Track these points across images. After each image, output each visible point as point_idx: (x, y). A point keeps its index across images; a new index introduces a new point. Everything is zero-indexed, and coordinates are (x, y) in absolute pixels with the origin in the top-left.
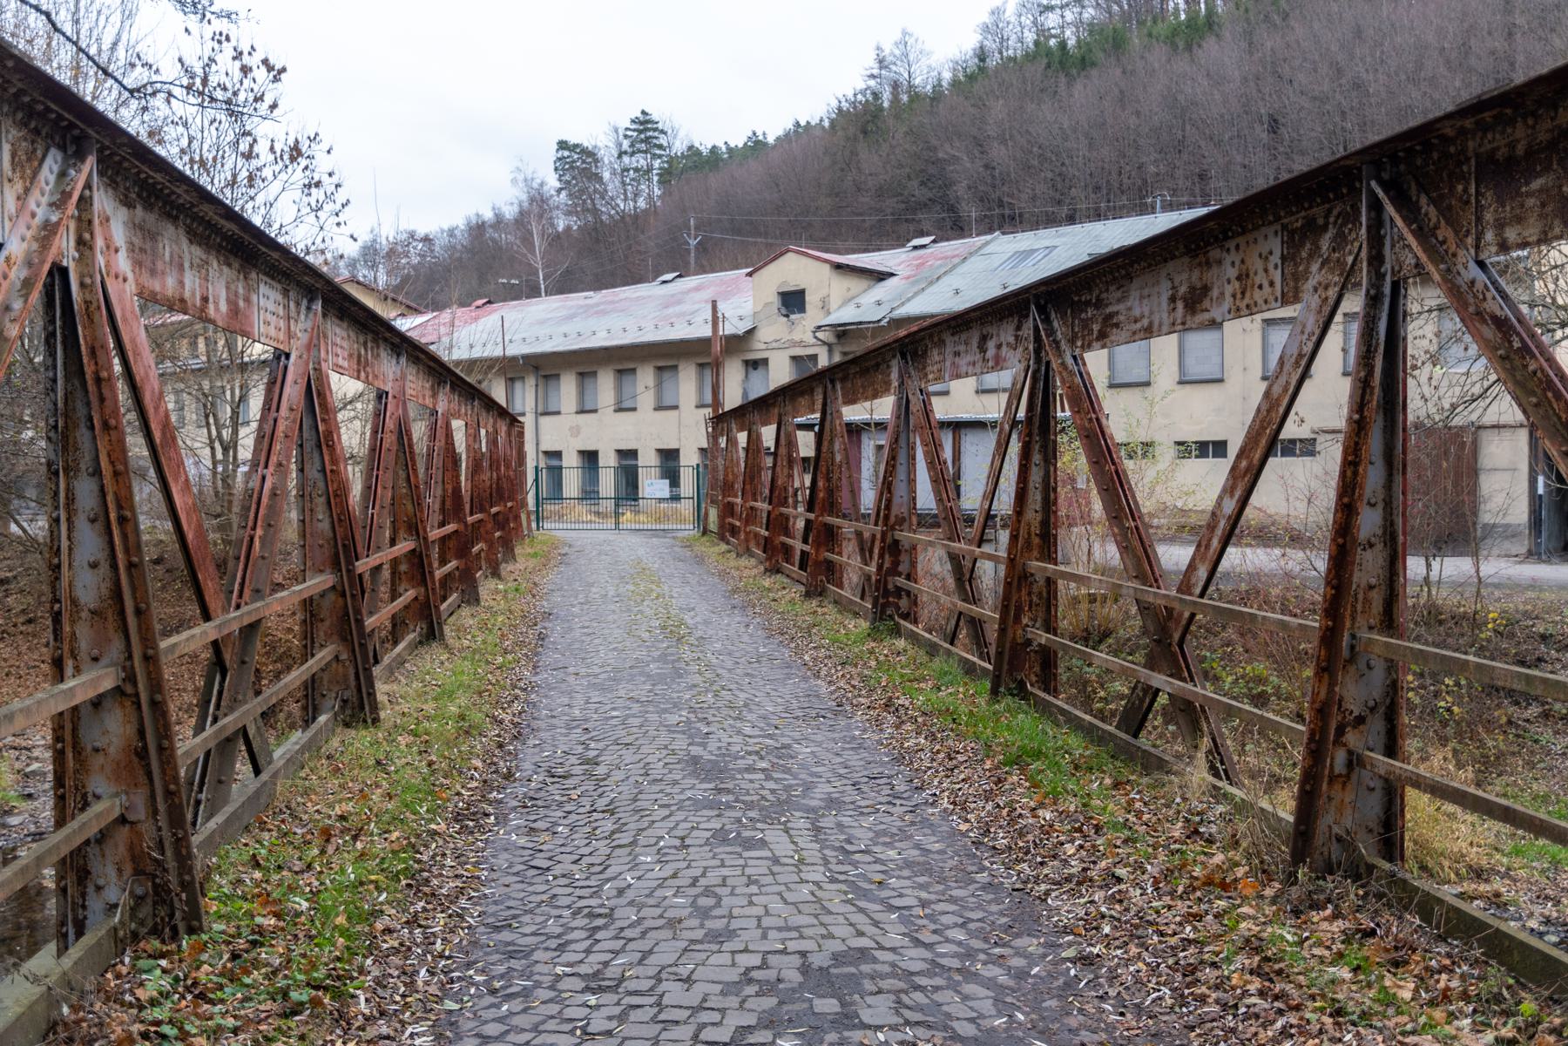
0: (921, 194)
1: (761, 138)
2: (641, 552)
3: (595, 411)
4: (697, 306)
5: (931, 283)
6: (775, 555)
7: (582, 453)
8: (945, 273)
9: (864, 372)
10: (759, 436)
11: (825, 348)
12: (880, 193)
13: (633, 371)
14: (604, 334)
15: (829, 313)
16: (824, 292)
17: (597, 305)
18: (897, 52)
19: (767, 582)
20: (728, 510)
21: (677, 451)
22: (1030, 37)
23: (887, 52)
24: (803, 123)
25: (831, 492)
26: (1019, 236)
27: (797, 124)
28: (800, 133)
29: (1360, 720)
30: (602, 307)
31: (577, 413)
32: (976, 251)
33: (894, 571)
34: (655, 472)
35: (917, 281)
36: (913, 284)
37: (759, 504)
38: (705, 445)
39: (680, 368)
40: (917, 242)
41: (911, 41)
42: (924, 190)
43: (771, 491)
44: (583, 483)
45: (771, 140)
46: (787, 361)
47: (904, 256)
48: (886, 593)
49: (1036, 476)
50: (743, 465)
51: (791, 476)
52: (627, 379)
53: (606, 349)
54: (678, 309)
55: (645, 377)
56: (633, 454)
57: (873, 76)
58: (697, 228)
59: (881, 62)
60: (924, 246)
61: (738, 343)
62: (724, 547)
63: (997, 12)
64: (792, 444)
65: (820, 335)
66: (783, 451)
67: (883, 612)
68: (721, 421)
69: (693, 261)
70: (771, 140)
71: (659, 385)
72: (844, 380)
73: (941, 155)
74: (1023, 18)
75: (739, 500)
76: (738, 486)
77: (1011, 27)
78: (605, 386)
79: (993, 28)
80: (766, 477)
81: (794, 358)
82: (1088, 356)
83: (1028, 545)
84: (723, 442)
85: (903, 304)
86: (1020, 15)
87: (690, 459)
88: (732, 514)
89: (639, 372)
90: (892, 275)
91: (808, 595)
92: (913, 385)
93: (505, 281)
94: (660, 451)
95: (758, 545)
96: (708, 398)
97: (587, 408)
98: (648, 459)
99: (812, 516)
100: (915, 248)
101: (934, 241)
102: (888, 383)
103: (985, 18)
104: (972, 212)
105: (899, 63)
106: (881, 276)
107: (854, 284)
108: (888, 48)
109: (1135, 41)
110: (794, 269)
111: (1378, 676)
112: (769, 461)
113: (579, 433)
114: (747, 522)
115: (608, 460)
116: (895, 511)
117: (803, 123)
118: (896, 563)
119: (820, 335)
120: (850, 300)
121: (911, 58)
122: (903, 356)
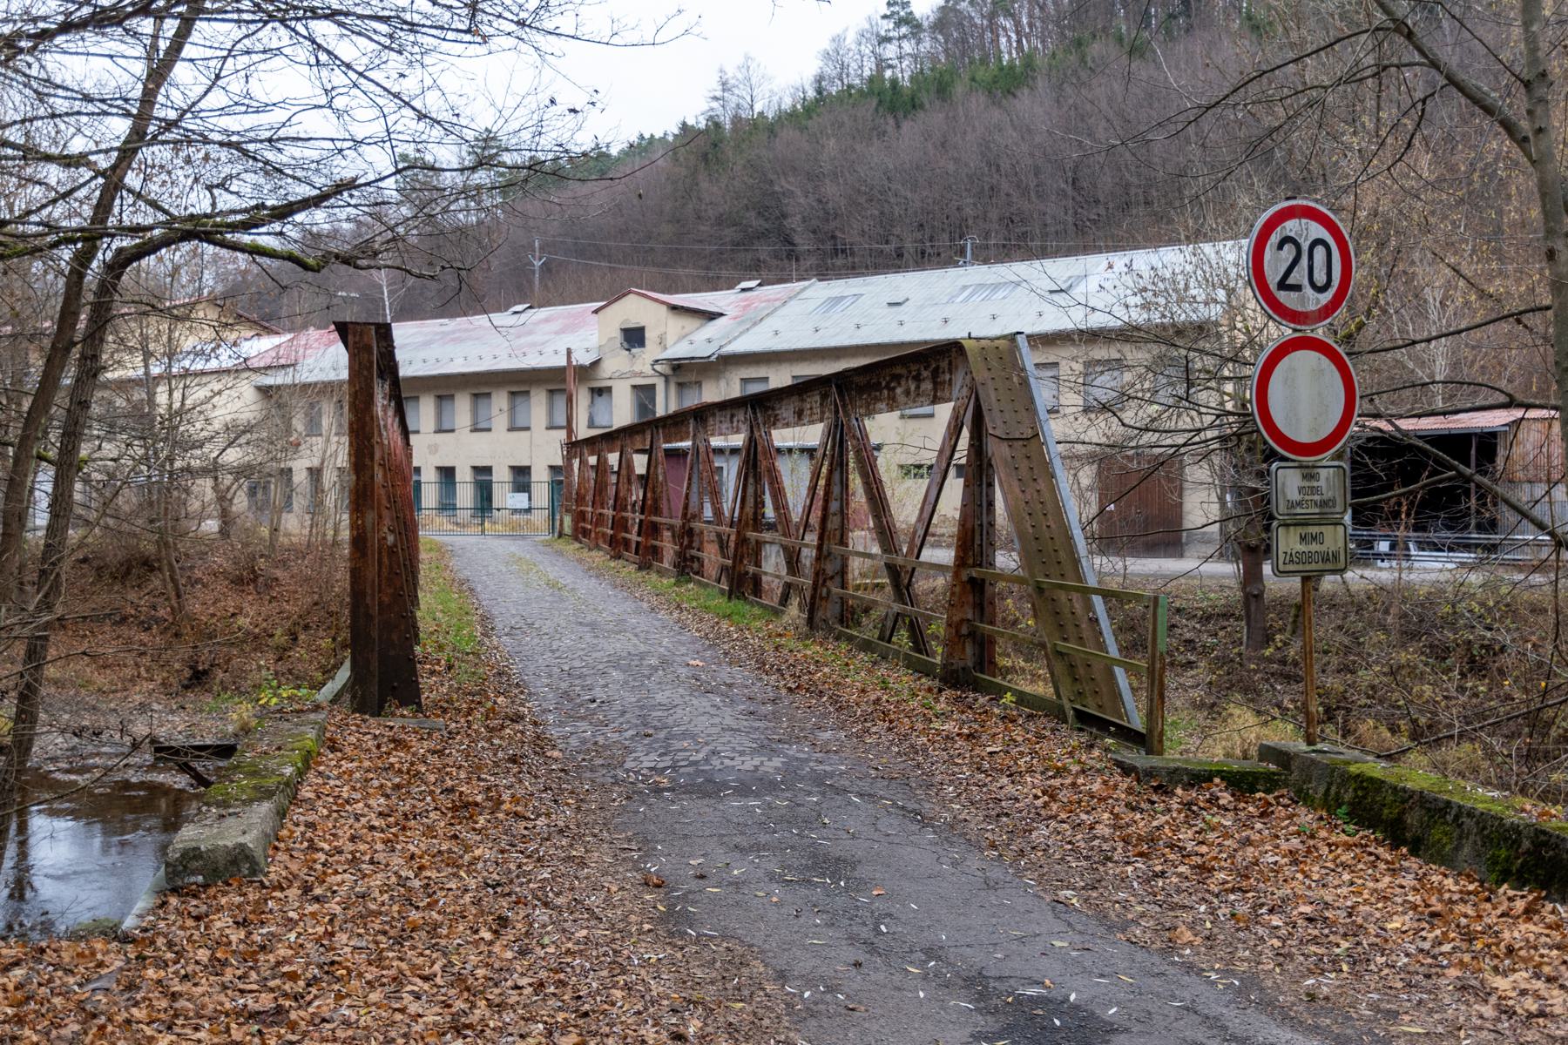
0: (757, 223)
1: (604, 150)
2: (512, 549)
3: (452, 431)
4: (546, 338)
5: (755, 324)
6: (617, 546)
7: (440, 469)
8: (768, 315)
9: (676, 424)
10: (606, 460)
11: (663, 379)
12: (720, 221)
13: (488, 395)
14: (459, 361)
15: (665, 348)
16: (662, 330)
17: (454, 332)
18: (740, 76)
19: (612, 564)
20: (580, 517)
21: (529, 468)
22: (869, 68)
23: (730, 75)
24: (647, 136)
25: (655, 500)
26: (833, 283)
27: (642, 137)
28: (643, 148)
29: (832, 578)
30: (457, 335)
31: (435, 432)
32: (795, 296)
33: (690, 546)
34: (508, 487)
35: (743, 322)
36: (740, 324)
37: (605, 511)
38: (559, 462)
39: (532, 393)
40: (744, 285)
41: (753, 66)
42: (761, 221)
43: (615, 501)
44: (441, 497)
45: (614, 151)
46: (629, 390)
47: (733, 298)
48: (685, 560)
49: (750, 490)
50: (592, 482)
51: (629, 490)
52: (482, 402)
53: (463, 375)
54: (529, 339)
55: (500, 401)
56: (488, 470)
57: (716, 98)
58: (542, 248)
59: (725, 86)
60: (750, 289)
61: (586, 373)
62: (577, 545)
63: (838, 40)
64: (630, 467)
65: (658, 367)
66: (624, 472)
67: (683, 570)
68: (574, 447)
69: (537, 283)
70: (614, 151)
71: (512, 409)
72: (664, 427)
73: (777, 188)
74: (863, 47)
75: (590, 509)
76: (589, 498)
77: (851, 54)
78: (462, 407)
79: (834, 55)
80: (612, 491)
81: (634, 387)
82: (773, 432)
83: (747, 524)
84: (576, 463)
85: (730, 342)
86: (860, 44)
87: (540, 476)
88: (584, 520)
89: (494, 397)
90: (722, 315)
91: (640, 569)
92: (701, 436)
93: (344, 294)
94: (513, 468)
95: (605, 542)
96: (561, 420)
97: (445, 427)
98: (502, 475)
99: (643, 517)
100: (743, 290)
101: (760, 285)
102: (688, 433)
103: (827, 45)
104: (803, 243)
105: (741, 86)
106: (712, 316)
107: (689, 323)
108: (731, 72)
109: (959, 89)
110: (635, 309)
111: (838, 562)
112: (614, 479)
113: (436, 451)
114: (596, 525)
115: (464, 476)
116: (691, 511)
117: (647, 136)
118: (691, 542)
119: (658, 367)
120: (684, 337)
121: (753, 81)
122: (695, 419)
